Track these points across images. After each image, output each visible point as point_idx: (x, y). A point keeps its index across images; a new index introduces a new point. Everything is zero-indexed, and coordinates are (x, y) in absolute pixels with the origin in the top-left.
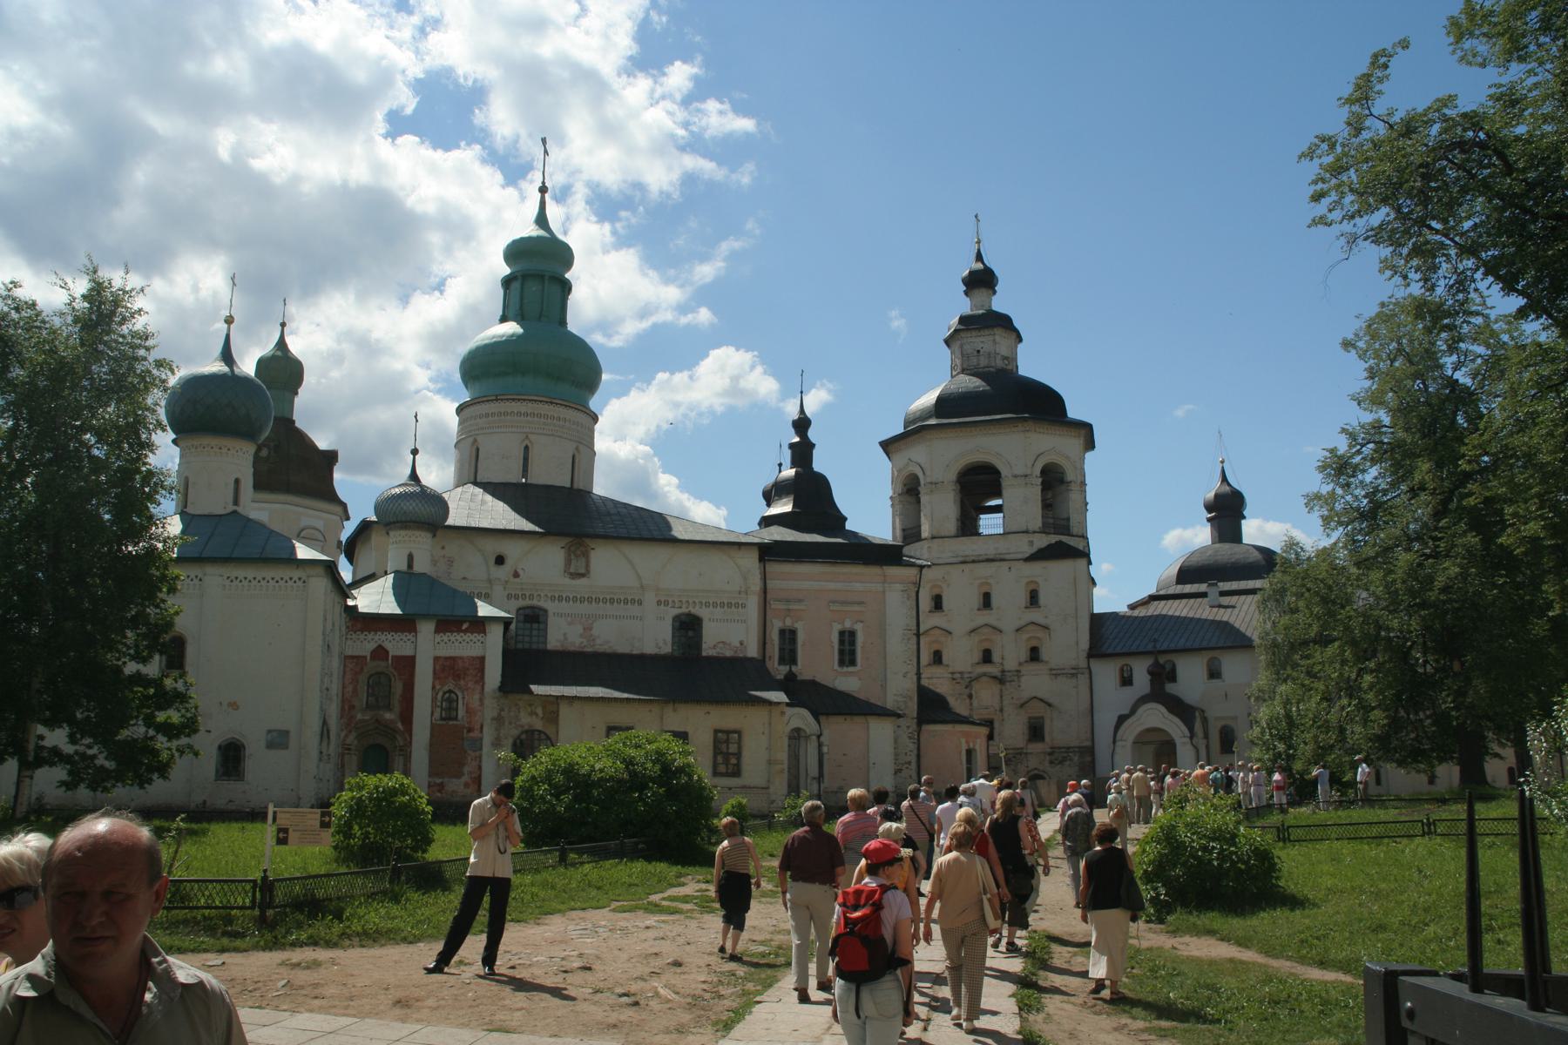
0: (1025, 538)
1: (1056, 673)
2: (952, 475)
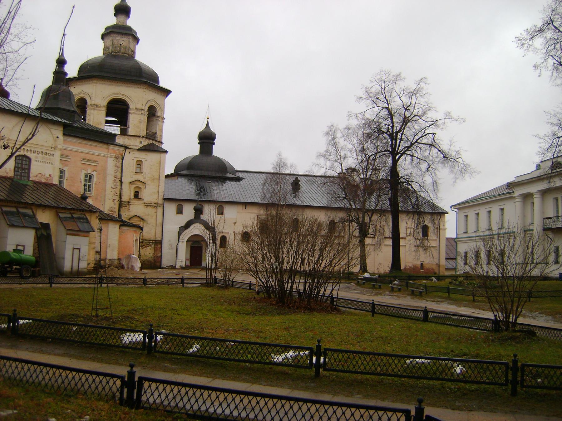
0: (138, 140)
1: (148, 205)
2: (105, 103)
